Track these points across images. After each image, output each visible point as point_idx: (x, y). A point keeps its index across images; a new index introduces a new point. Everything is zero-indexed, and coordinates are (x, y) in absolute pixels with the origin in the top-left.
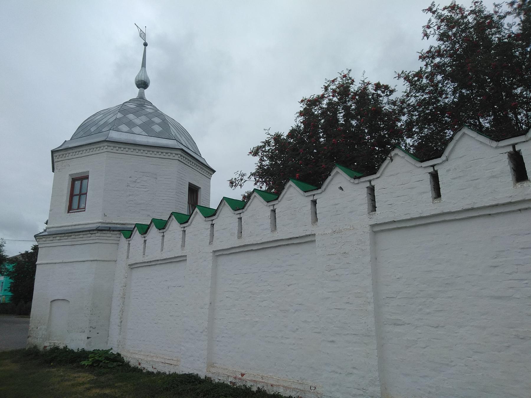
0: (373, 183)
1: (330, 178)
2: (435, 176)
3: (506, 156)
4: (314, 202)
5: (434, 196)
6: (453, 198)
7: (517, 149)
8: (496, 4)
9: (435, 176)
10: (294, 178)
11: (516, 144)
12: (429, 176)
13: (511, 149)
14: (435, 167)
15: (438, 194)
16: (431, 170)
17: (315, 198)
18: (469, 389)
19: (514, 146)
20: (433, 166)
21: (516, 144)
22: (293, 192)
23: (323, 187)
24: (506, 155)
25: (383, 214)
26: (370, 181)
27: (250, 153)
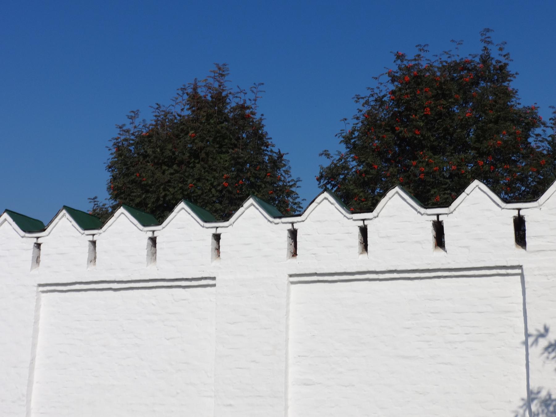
0: (296, 226)
1: (241, 210)
2: (364, 231)
3: (431, 224)
4: (217, 237)
5: (361, 251)
6: (378, 257)
7: (440, 220)
8: (120, 125)
9: (364, 231)
10: (256, 197)
11: (440, 214)
12: (358, 230)
13: (435, 218)
14: (521, 211)
15: (93, 259)
16: (361, 223)
17: (219, 231)
18: (286, 408)
19: (438, 215)
20: (363, 220)
21: (440, 214)
22: (396, 205)
23: (232, 220)
24: (432, 222)
25: (305, 262)
26: (153, 231)
27: (516, 92)
